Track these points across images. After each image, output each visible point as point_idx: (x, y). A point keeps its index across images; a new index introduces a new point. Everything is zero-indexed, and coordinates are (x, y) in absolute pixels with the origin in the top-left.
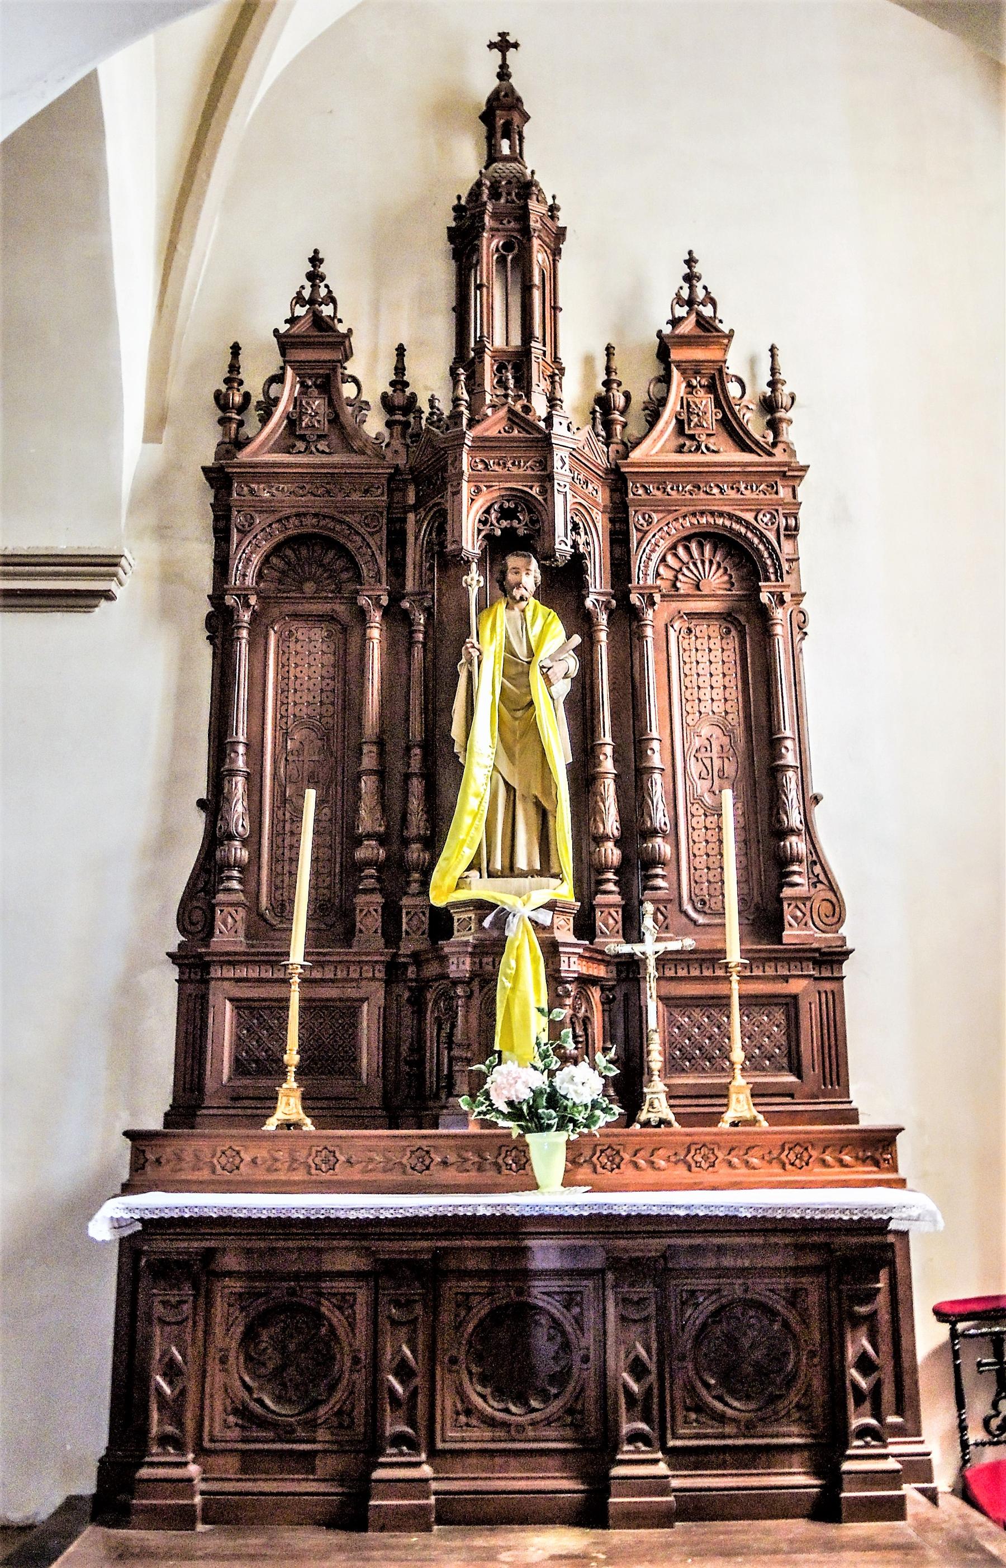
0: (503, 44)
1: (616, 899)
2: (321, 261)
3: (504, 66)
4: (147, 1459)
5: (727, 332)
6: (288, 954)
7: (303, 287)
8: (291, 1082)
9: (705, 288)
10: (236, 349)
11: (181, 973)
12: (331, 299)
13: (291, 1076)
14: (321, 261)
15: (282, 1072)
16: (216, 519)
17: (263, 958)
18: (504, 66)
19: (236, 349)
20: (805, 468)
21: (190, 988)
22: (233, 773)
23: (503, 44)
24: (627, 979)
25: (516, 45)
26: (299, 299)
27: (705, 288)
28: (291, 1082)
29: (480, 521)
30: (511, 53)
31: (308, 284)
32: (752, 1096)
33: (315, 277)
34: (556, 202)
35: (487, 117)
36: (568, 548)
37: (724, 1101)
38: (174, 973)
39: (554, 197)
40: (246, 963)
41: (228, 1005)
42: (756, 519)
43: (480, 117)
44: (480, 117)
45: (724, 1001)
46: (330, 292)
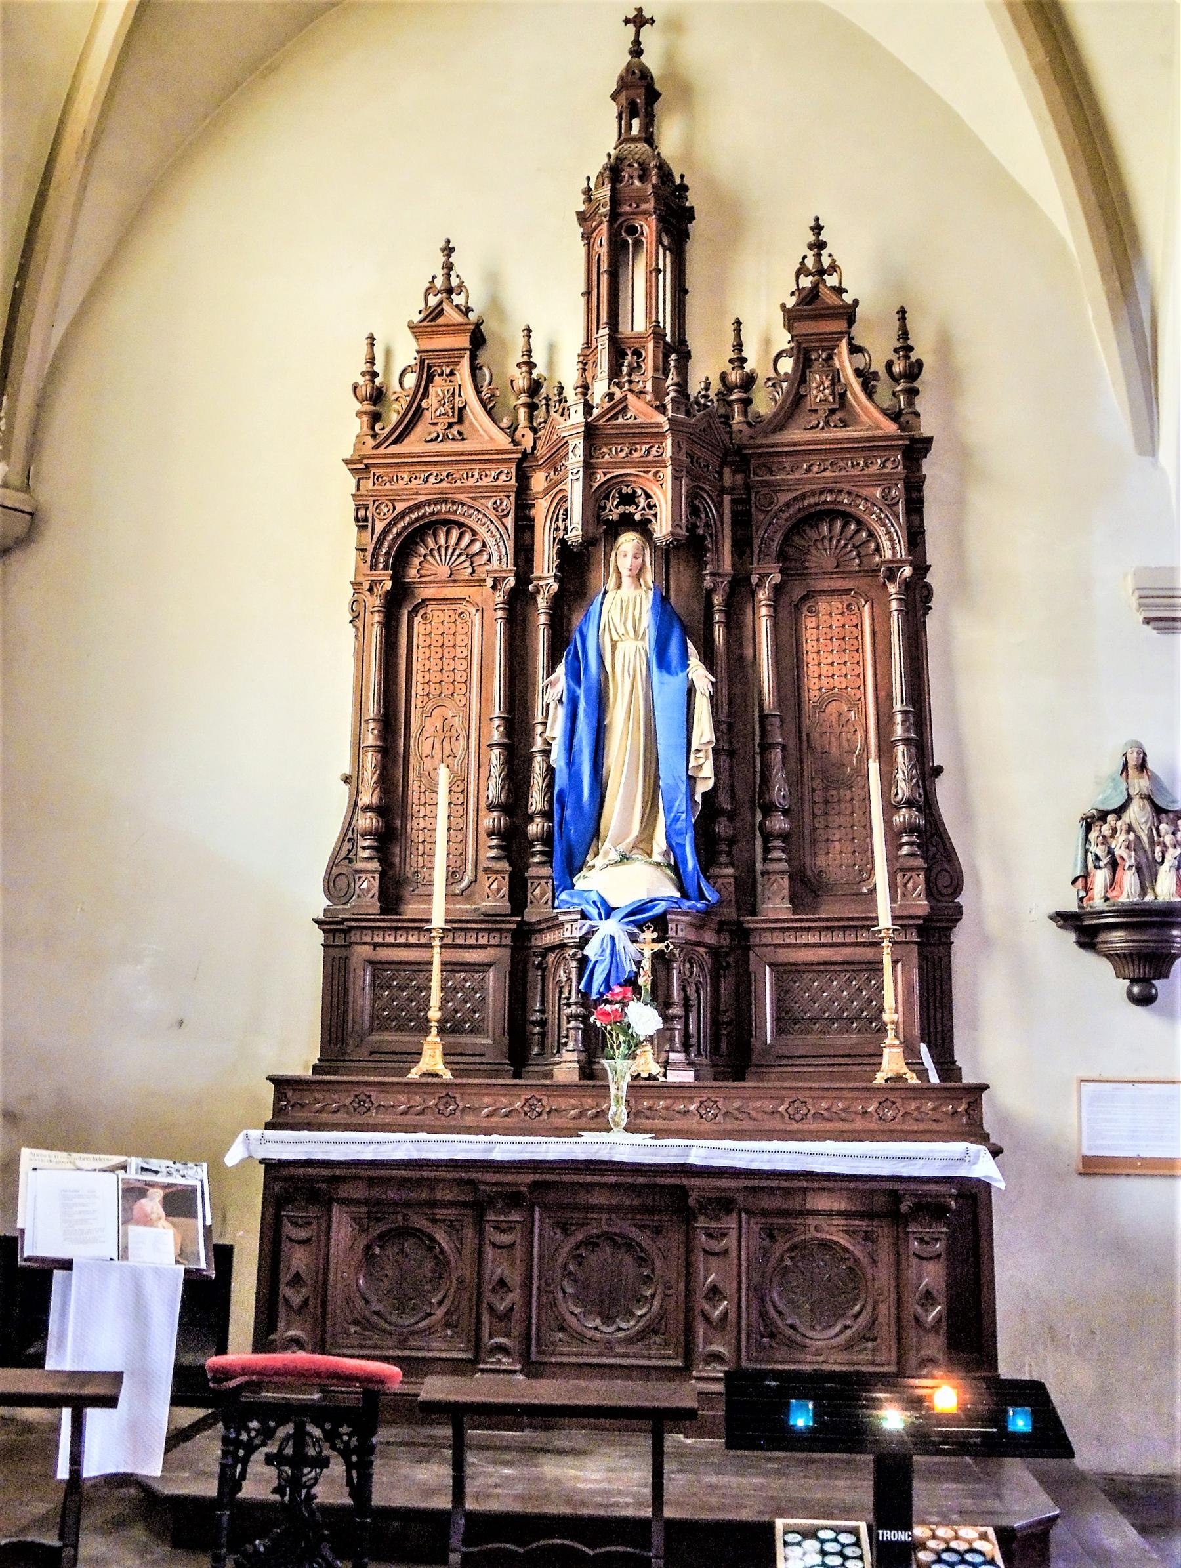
0: (639, 20)
1: (784, 866)
2: (821, 228)
3: (637, 42)
4: (481, 1366)
5: (850, 302)
6: (876, 918)
7: (805, 257)
8: (433, 1037)
9: (830, 255)
10: (902, 312)
11: (326, 938)
12: (834, 268)
13: (434, 1031)
14: (821, 228)
15: (882, 1030)
16: (920, 489)
17: (821, 924)
18: (637, 42)
19: (902, 312)
20: (929, 440)
21: (336, 952)
22: (907, 741)
23: (639, 20)
24: (739, 947)
25: (627, 21)
26: (802, 271)
27: (830, 255)
28: (433, 1037)
29: (655, 506)
30: (646, 29)
31: (810, 254)
32: (445, 1055)
33: (819, 246)
34: (685, 182)
35: (653, 95)
36: (684, 532)
37: (876, 1060)
38: (319, 936)
39: (682, 177)
40: (845, 928)
41: (767, 968)
42: (507, 515)
43: (660, 95)
44: (660, 95)
45: (876, 966)
46: (834, 261)
